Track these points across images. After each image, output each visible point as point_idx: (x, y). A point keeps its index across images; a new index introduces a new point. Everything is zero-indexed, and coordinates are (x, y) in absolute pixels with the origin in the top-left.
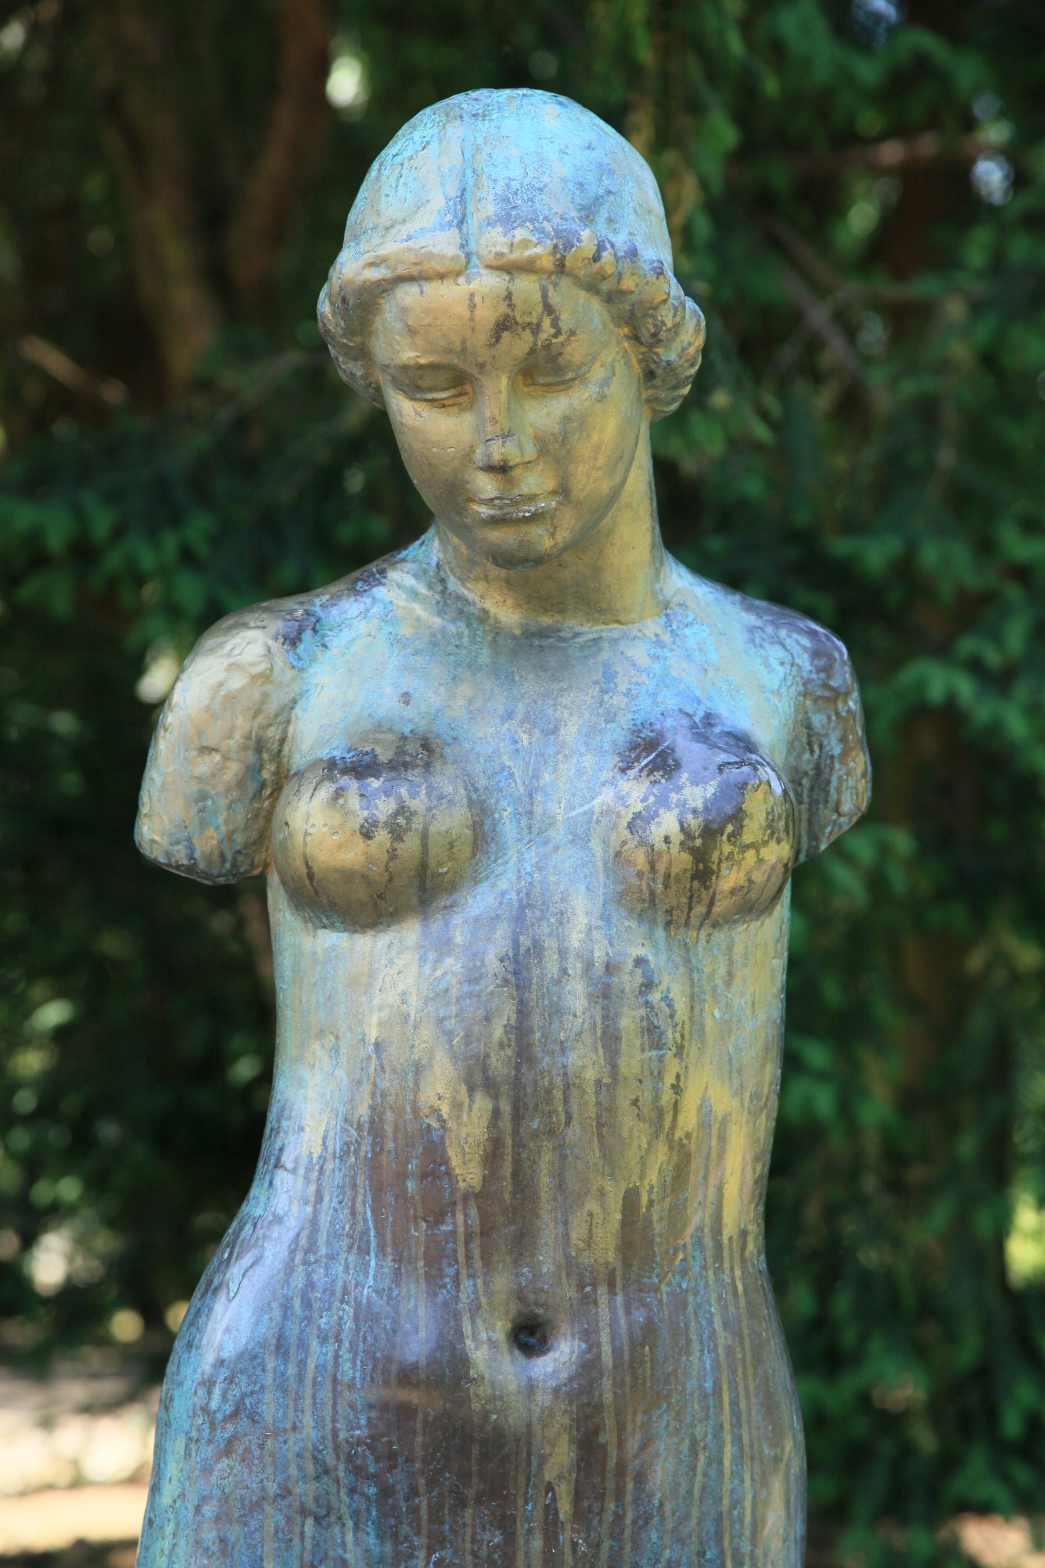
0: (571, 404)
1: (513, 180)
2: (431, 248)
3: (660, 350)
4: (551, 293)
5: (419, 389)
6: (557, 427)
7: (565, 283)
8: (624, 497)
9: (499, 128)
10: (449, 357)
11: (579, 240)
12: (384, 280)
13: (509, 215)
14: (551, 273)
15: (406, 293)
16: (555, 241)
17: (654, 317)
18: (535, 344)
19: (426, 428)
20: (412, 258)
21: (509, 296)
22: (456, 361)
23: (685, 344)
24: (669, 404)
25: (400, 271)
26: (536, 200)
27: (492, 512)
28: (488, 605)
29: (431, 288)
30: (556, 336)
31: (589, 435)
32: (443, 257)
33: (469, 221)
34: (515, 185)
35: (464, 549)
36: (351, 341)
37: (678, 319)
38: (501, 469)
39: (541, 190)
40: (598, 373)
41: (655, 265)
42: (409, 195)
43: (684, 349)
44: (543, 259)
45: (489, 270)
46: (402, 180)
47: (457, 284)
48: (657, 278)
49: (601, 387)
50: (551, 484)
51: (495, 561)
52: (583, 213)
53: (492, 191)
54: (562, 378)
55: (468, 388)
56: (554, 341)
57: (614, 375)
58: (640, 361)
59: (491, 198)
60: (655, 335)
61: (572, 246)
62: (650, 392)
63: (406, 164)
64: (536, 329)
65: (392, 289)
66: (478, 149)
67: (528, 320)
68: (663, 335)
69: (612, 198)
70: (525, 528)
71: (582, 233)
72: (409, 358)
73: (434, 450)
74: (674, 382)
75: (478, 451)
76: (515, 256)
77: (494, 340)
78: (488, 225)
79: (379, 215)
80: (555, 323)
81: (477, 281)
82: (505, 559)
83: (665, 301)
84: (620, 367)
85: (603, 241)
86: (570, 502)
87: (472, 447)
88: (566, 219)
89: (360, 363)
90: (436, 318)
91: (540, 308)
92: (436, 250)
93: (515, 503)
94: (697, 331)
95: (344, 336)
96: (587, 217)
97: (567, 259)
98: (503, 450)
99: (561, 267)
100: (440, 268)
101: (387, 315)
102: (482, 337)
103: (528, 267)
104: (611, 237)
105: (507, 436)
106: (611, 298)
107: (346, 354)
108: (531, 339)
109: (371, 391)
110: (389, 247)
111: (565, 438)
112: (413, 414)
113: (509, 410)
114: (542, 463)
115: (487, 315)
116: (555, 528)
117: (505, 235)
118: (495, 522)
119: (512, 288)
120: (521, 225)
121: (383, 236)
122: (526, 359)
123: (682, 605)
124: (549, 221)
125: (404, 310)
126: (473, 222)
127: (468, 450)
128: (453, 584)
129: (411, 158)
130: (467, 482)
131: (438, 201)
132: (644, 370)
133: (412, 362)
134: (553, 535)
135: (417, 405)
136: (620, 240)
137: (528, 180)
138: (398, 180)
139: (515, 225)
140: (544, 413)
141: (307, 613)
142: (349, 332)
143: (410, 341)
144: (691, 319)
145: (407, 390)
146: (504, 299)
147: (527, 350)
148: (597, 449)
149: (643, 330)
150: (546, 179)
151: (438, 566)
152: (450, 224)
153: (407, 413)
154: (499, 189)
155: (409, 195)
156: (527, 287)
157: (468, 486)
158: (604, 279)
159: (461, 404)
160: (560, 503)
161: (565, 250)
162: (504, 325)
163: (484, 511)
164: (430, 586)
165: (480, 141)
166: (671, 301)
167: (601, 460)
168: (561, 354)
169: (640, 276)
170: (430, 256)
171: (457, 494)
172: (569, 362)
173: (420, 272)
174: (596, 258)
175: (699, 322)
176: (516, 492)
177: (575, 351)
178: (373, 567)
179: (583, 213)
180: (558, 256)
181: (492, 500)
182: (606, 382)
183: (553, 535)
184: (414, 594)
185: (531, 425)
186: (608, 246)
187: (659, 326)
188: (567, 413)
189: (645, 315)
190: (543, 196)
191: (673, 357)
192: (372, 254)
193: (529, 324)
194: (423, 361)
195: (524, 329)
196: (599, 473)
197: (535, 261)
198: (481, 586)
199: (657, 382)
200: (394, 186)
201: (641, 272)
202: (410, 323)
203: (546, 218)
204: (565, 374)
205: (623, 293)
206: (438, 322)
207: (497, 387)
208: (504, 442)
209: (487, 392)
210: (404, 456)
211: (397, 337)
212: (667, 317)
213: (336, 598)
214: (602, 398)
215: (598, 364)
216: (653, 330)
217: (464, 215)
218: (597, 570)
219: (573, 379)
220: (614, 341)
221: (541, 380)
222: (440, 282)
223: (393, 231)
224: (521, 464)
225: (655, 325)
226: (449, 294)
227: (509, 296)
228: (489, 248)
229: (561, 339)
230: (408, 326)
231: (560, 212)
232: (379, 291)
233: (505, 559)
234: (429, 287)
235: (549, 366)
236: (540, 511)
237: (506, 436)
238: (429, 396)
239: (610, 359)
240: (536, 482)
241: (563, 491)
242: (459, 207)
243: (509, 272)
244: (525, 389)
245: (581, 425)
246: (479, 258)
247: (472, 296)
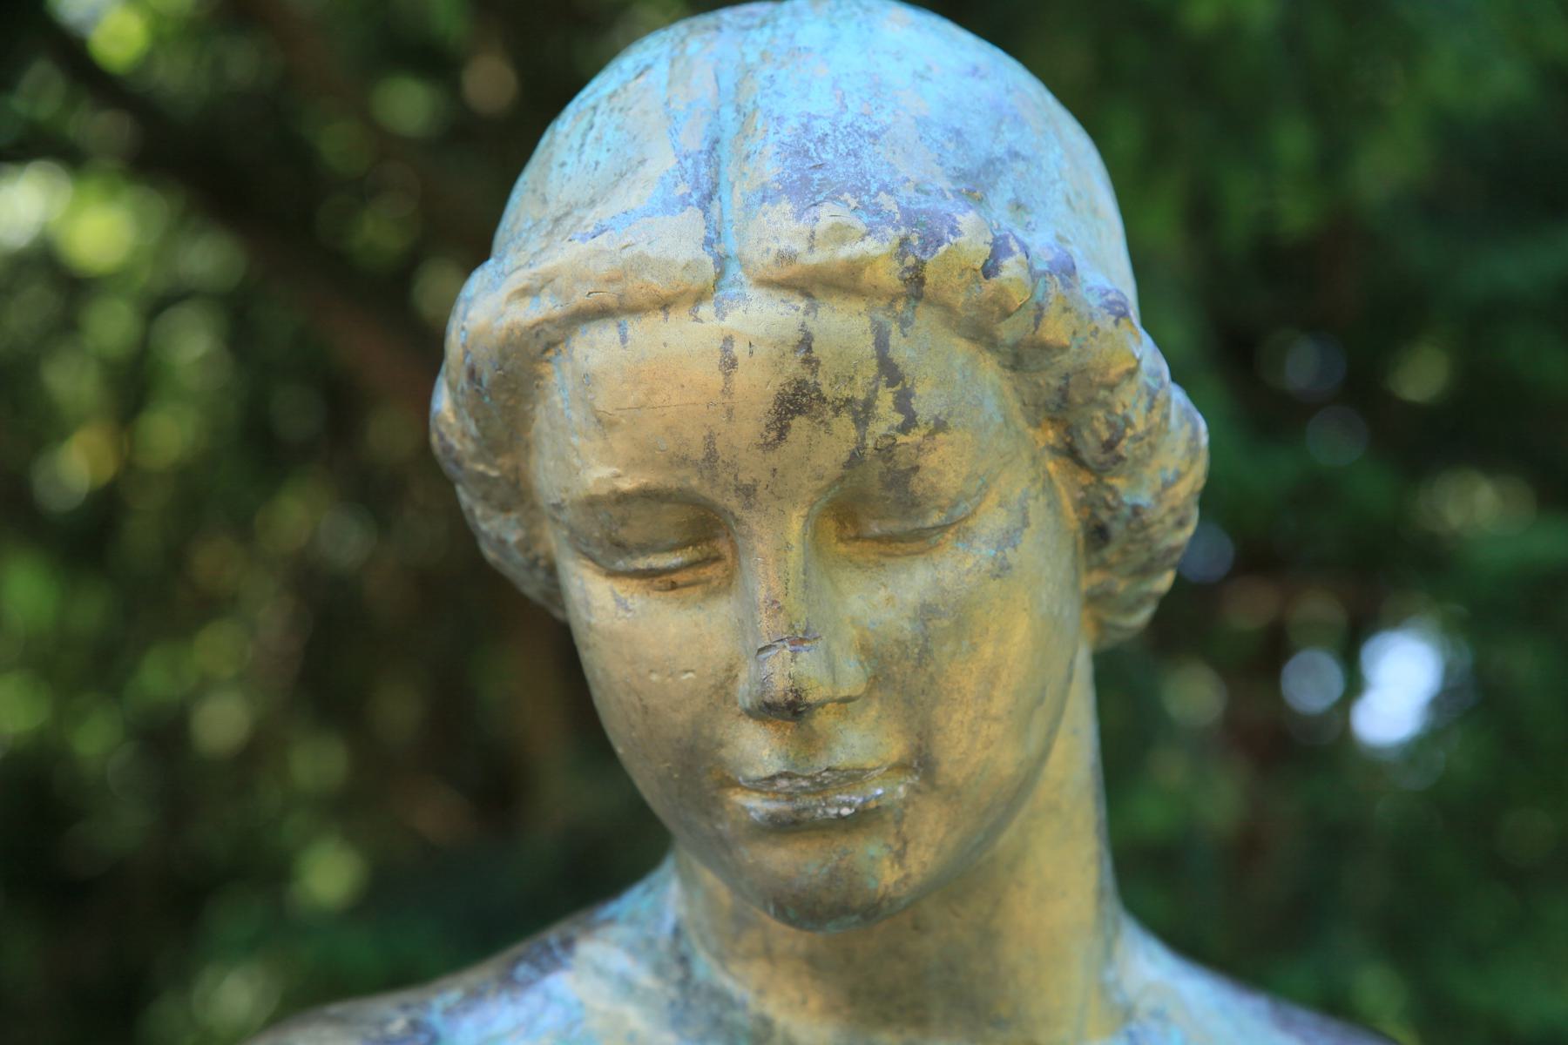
0: (936, 581)
1: (816, 118)
2: (642, 247)
3: (1119, 483)
4: (895, 339)
5: (621, 547)
6: (907, 626)
7: (925, 318)
8: (1045, 790)
9: (792, 37)
10: (681, 473)
11: (954, 231)
12: (548, 321)
13: (806, 181)
14: (894, 298)
15: (592, 345)
16: (903, 231)
17: (1107, 405)
18: (861, 446)
19: (635, 631)
20: (603, 268)
21: (806, 342)
22: (694, 482)
23: (1170, 474)
24: (1131, 609)
25: (580, 298)
26: (865, 153)
27: (773, 807)
28: (772, 1007)
29: (647, 332)
30: (905, 429)
31: (974, 647)
32: (668, 264)
33: (725, 198)
34: (821, 127)
35: (724, 896)
36: (491, 465)
37: (1156, 417)
38: (789, 711)
39: (874, 136)
40: (992, 520)
41: (1111, 297)
42: (603, 157)
43: (1167, 485)
44: (880, 263)
45: (763, 291)
46: (593, 133)
47: (697, 319)
48: (1117, 323)
49: (1000, 547)
50: (895, 749)
51: (781, 913)
52: (963, 186)
53: (772, 138)
54: (919, 524)
55: (723, 546)
56: (901, 439)
57: (1026, 524)
58: (1080, 505)
59: (770, 150)
60: (1109, 446)
61: (940, 243)
62: (1097, 577)
63: (604, 106)
64: (863, 413)
65: (565, 339)
66: (748, 71)
67: (847, 393)
68: (1125, 447)
69: (1020, 166)
70: (841, 842)
71: (959, 218)
72: (599, 480)
73: (654, 677)
74: (1144, 557)
75: (743, 676)
76: (818, 258)
77: (774, 434)
78: (763, 199)
79: (545, 201)
80: (903, 402)
81: (739, 312)
82: (803, 909)
83: (1131, 373)
84: (1038, 510)
85: (1006, 237)
86: (934, 787)
87: (730, 668)
88: (927, 193)
89: (514, 516)
90: (652, 391)
91: (871, 369)
92: (652, 252)
93: (820, 787)
94: (1193, 450)
95: (478, 457)
96: (970, 192)
97: (929, 268)
98: (793, 669)
99: (915, 284)
100: (662, 287)
101: (557, 398)
102: (749, 428)
103: (840, 283)
104: (1019, 233)
105: (802, 640)
106: (1022, 358)
107: (486, 498)
108: (853, 433)
109: (540, 575)
110: (564, 255)
111: (925, 651)
112: (611, 605)
113: (806, 585)
114: (876, 704)
115: (758, 384)
116: (905, 843)
117: (799, 217)
118: (782, 828)
119: (812, 326)
120: (833, 199)
121: (550, 233)
122: (842, 478)
123: (1159, 1015)
124: (890, 193)
125: (588, 380)
126: (731, 202)
127: (722, 675)
128: (704, 967)
129: (611, 96)
130: (721, 745)
131: (662, 162)
132: (1086, 524)
133: (604, 490)
134: (900, 857)
135: (620, 587)
136: (1041, 242)
137: (847, 118)
138: (585, 135)
139: (819, 198)
140: (881, 599)
141: (415, 1026)
142: (491, 446)
143: (600, 444)
144: (1181, 426)
145: (598, 553)
146: (795, 349)
147: (845, 457)
148: (991, 677)
149: (1086, 433)
150: (885, 117)
151: (677, 932)
152: (684, 201)
153: (600, 603)
154: (786, 134)
155: (603, 157)
156: (844, 326)
157: (723, 752)
158: (1007, 314)
159: (708, 581)
160: (915, 790)
161: (924, 251)
162: (796, 403)
163: (757, 805)
164: (659, 970)
165: (752, 58)
166: (1142, 377)
167: (1000, 702)
168: (916, 469)
169: (1079, 317)
170: (643, 262)
171: (702, 770)
172: (933, 487)
173: (620, 296)
174: (989, 270)
175: (1195, 430)
176: (822, 762)
177: (945, 466)
178: (552, 936)
179: (963, 186)
180: (910, 261)
181: (772, 779)
182: (1009, 539)
183: (900, 857)
184: (627, 986)
185: (853, 621)
186: (1016, 248)
187: (1120, 427)
188: (929, 598)
189: (1091, 401)
190: (877, 148)
191: (1144, 498)
192: (526, 272)
193: (849, 401)
194: (626, 485)
195: (837, 411)
196: (996, 730)
197: (861, 270)
198: (758, 970)
199: (1111, 553)
200: (576, 145)
201: (1083, 309)
202: (599, 405)
203: (884, 187)
204: (924, 515)
205: (1045, 349)
206: (658, 399)
207: (777, 545)
208: (794, 652)
209: (761, 548)
210: (597, 694)
211: (575, 440)
212: (1130, 401)
213: (475, 996)
214: (1002, 570)
215: (992, 499)
216: (1106, 435)
217: (716, 185)
218: (988, 937)
219: (942, 528)
220: (1025, 455)
221: (875, 528)
222: (661, 315)
223: (569, 222)
224: (832, 700)
225: (1111, 425)
226: (685, 338)
227: (806, 342)
228: (764, 245)
229: (915, 437)
230: (595, 412)
231: (914, 178)
232: (539, 348)
233: (803, 909)
234: (638, 329)
235: (892, 494)
236: (873, 805)
237: (799, 640)
238: (642, 563)
239: (1018, 492)
240: (863, 742)
241: (921, 763)
242: (703, 170)
243: (806, 293)
244: (842, 548)
245: (959, 624)
246: (744, 265)
247: (728, 340)
